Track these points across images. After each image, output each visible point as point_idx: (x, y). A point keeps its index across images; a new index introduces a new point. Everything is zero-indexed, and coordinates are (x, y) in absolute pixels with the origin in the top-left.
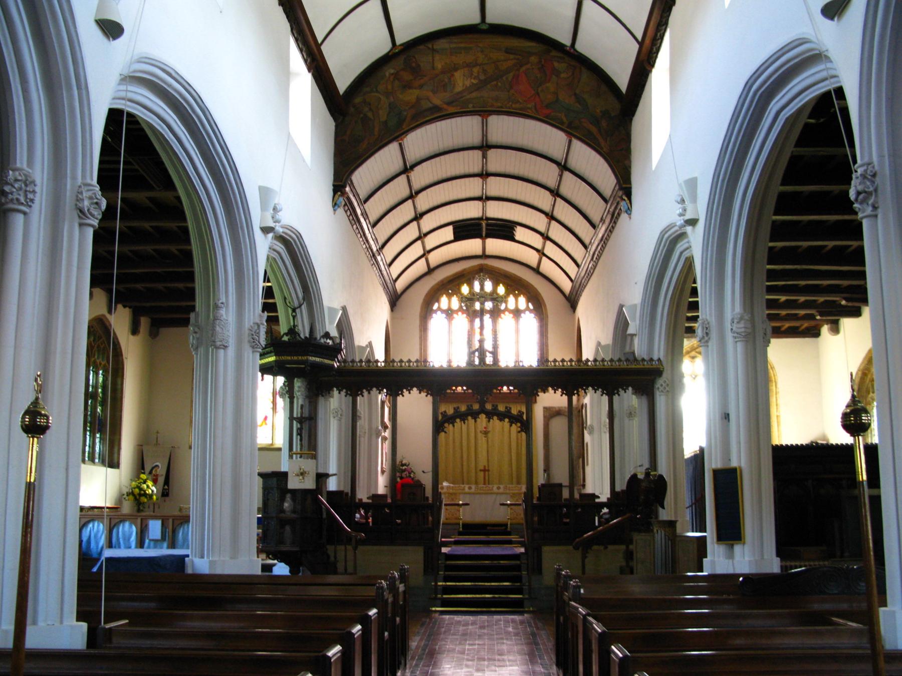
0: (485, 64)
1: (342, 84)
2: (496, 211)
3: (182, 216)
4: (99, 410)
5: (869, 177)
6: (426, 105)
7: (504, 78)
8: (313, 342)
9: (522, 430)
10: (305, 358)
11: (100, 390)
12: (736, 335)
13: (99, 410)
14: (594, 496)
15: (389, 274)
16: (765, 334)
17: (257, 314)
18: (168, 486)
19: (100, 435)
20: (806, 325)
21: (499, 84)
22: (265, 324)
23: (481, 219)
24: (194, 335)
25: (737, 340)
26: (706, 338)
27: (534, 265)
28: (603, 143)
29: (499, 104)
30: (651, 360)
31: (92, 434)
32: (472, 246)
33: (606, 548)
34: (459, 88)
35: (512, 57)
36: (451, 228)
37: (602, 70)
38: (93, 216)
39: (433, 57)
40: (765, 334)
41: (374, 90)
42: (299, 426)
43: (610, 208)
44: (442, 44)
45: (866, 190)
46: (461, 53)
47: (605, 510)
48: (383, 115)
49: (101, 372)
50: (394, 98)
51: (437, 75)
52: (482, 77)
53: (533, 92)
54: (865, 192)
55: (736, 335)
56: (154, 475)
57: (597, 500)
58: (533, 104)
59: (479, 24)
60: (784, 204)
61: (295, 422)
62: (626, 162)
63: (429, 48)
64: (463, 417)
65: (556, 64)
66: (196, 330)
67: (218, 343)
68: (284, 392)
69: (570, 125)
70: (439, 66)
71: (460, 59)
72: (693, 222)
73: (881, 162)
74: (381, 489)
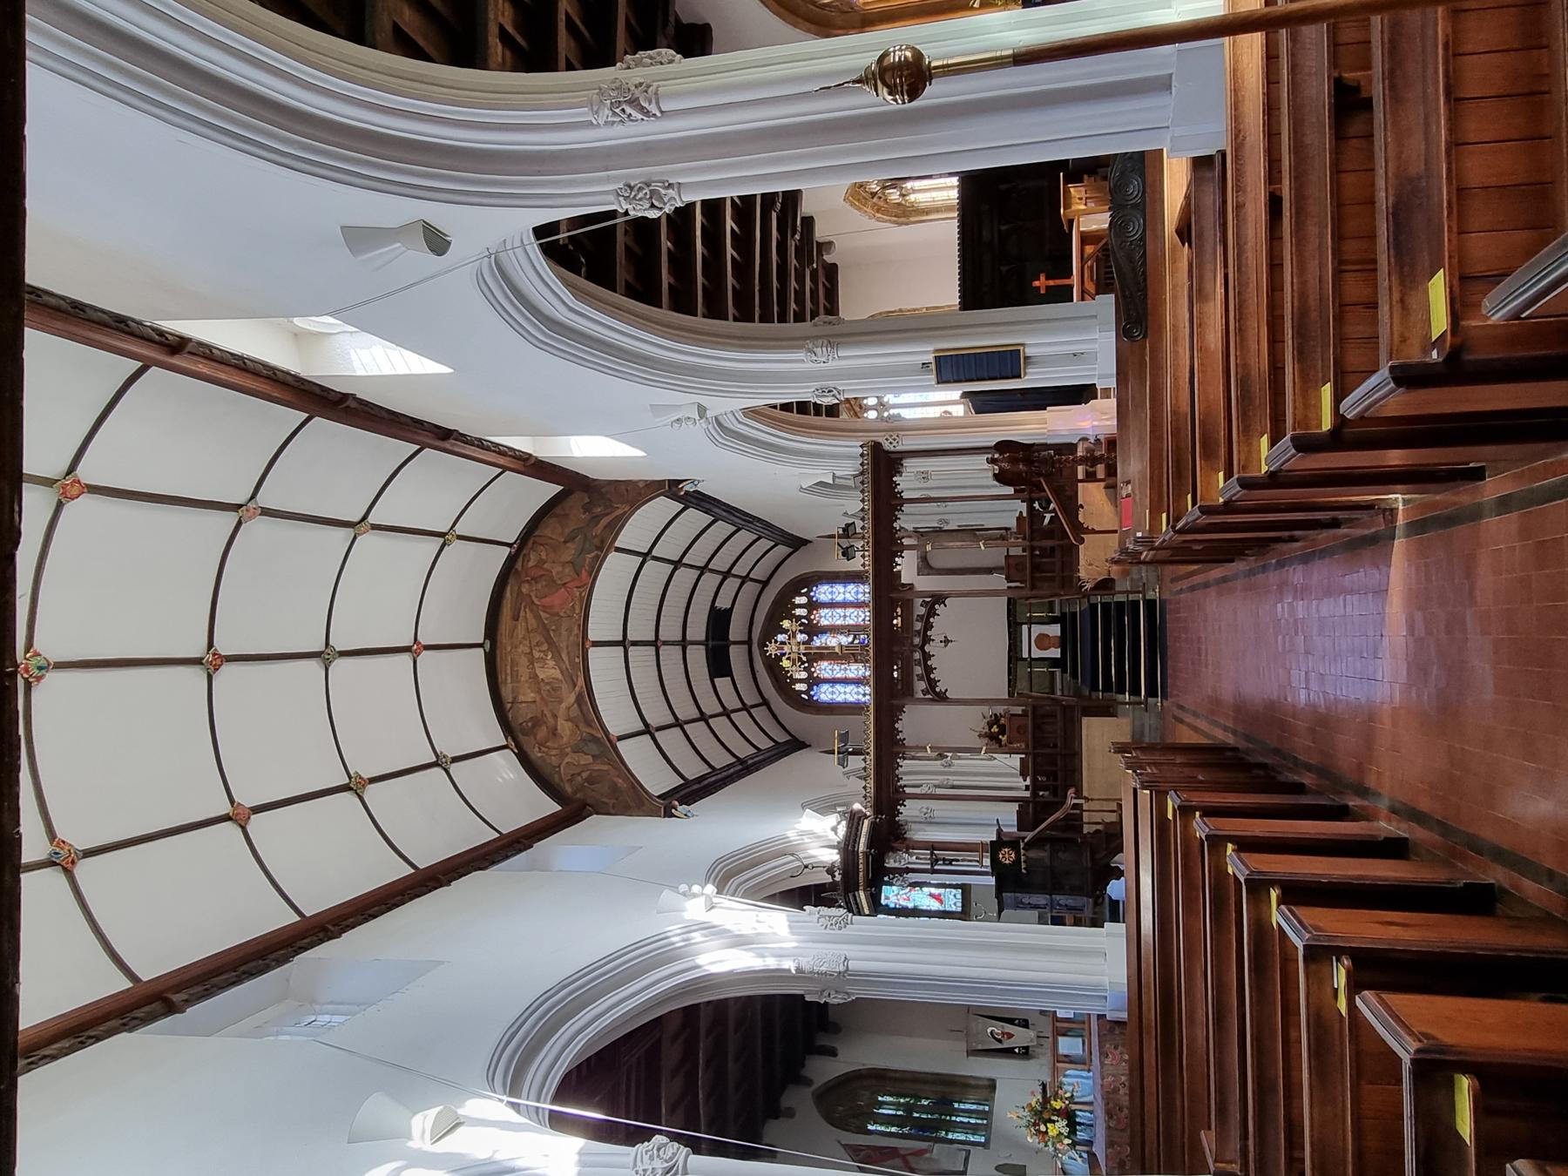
0: (530, 643)
1: (549, 807)
2: (698, 630)
3: (695, 1008)
4: (925, 1102)
5: (633, 193)
6: (575, 712)
7: (546, 622)
8: (842, 845)
9: (944, 603)
10: (860, 854)
11: (902, 1101)
12: (830, 358)
13: (926, 1103)
14: (1020, 519)
15: (769, 750)
16: (830, 323)
17: (808, 919)
18: (1016, 1019)
19: (956, 1102)
20: (822, 279)
21: (553, 628)
22: (819, 908)
23: (707, 646)
24: (832, 996)
25: (836, 356)
26: (835, 392)
27: (759, 586)
28: (620, 512)
29: (576, 628)
30: (862, 455)
31: (956, 1113)
32: (737, 655)
33: (1082, 506)
34: (557, 673)
35: (522, 614)
36: (716, 680)
37: (1538, 380)
38: (674, 1154)
39: (522, 702)
40: (830, 323)
41: (557, 769)
42: (941, 862)
43: (692, 503)
44: (506, 692)
45: (648, 197)
46: (518, 671)
47: (1036, 505)
48: (586, 760)
49: (880, 1098)
50: (567, 747)
51: (542, 698)
52: (545, 647)
53: (563, 590)
54: (651, 198)
55: (830, 358)
56: (1003, 1037)
57: (1025, 515)
58: (575, 589)
59: (485, 650)
60: (682, 303)
61: (936, 867)
62: (641, 485)
63: (511, 708)
64: (929, 670)
65: (531, 564)
66: (826, 993)
67: (842, 968)
68: (901, 879)
69: (600, 548)
70: (531, 696)
71: (524, 673)
72: (702, 410)
73: (616, 179)
74: (1015, 761)
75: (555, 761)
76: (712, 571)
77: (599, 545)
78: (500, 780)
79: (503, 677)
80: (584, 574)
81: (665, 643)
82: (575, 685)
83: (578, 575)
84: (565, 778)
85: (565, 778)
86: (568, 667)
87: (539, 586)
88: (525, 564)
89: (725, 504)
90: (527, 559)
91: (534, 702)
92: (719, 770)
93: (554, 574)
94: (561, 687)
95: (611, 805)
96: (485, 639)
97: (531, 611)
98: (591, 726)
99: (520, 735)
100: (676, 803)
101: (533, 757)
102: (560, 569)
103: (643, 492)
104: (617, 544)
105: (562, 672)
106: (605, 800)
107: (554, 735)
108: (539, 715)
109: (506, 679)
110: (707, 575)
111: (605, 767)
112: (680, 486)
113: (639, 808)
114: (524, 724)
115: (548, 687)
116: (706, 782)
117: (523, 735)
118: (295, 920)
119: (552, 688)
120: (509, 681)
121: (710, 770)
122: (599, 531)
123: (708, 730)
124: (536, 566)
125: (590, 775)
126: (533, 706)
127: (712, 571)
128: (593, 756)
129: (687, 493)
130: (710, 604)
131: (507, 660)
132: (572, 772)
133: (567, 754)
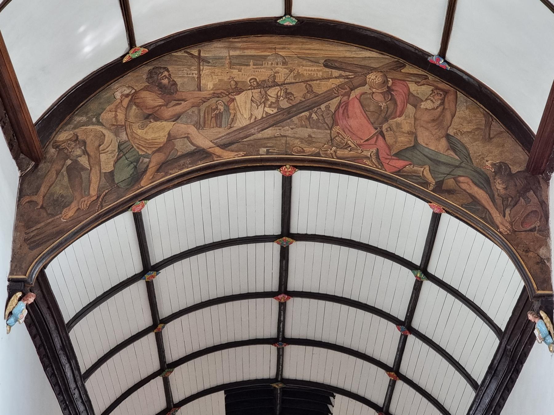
6: (182, 147)
7: (323, 107)
23: (275, 380)
28: (497, 217)
34: (242, 121)
35: (336, 73)
36: (221, 396)
41: (94, 119)
52: (285, 104)
53: (374, 131)
59: (281, 17)
63: (192, 56)
65: (413, 87)
75: (107, 116)
76: (392, 386)
77: (444, 187)
78: (82, 29)
79: (239, 45)
80: (399, 164)
81: (282, 308)
82: (224, 146)
83: (396, 155)
84: (79, 132)
85: (79, 132)
86: (252, 138)
87: (378, 98)
88: (413, 78)
89: (504, 399)
90: (420, 80)
91: (200, 89)
92: (83, 386)
93: (398, 119)
94: (220, 127)
95: (34, 198)
96: (297, 18)
97: (341, 86)
98: (158, 171)
99: (150, 68)
100: (31, 300)
101: (115, 86)
102: (406, 128)
103: (531, 254)
104: (445, 218)
105: (242, 128)
106: (43, 190)
107: (147, 117)
108: (176, 96)
109: (235, 48)
110: (384, 378)
111: (93, 192)
112: (543, 314)
113: (25, 240)
114: (166, 73)
115: (221, 108)
116: (64, 360)
117: (150, 72)
118: (65, 322)
119: (221, 114)
120: (232, 53)
121: (83, 371)
122: (464, 186)
123: (144, 375)
124: (410, 93)
125: (83, 169)
126: (193, 86)
127: (392, 386)
128: (112, 173)
129: (531, 326)
130: (341, 385)
131: (266, 49)
132: (88, 141)
133: (117, 134)
